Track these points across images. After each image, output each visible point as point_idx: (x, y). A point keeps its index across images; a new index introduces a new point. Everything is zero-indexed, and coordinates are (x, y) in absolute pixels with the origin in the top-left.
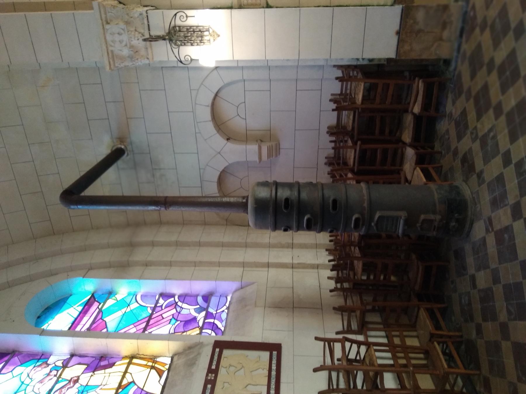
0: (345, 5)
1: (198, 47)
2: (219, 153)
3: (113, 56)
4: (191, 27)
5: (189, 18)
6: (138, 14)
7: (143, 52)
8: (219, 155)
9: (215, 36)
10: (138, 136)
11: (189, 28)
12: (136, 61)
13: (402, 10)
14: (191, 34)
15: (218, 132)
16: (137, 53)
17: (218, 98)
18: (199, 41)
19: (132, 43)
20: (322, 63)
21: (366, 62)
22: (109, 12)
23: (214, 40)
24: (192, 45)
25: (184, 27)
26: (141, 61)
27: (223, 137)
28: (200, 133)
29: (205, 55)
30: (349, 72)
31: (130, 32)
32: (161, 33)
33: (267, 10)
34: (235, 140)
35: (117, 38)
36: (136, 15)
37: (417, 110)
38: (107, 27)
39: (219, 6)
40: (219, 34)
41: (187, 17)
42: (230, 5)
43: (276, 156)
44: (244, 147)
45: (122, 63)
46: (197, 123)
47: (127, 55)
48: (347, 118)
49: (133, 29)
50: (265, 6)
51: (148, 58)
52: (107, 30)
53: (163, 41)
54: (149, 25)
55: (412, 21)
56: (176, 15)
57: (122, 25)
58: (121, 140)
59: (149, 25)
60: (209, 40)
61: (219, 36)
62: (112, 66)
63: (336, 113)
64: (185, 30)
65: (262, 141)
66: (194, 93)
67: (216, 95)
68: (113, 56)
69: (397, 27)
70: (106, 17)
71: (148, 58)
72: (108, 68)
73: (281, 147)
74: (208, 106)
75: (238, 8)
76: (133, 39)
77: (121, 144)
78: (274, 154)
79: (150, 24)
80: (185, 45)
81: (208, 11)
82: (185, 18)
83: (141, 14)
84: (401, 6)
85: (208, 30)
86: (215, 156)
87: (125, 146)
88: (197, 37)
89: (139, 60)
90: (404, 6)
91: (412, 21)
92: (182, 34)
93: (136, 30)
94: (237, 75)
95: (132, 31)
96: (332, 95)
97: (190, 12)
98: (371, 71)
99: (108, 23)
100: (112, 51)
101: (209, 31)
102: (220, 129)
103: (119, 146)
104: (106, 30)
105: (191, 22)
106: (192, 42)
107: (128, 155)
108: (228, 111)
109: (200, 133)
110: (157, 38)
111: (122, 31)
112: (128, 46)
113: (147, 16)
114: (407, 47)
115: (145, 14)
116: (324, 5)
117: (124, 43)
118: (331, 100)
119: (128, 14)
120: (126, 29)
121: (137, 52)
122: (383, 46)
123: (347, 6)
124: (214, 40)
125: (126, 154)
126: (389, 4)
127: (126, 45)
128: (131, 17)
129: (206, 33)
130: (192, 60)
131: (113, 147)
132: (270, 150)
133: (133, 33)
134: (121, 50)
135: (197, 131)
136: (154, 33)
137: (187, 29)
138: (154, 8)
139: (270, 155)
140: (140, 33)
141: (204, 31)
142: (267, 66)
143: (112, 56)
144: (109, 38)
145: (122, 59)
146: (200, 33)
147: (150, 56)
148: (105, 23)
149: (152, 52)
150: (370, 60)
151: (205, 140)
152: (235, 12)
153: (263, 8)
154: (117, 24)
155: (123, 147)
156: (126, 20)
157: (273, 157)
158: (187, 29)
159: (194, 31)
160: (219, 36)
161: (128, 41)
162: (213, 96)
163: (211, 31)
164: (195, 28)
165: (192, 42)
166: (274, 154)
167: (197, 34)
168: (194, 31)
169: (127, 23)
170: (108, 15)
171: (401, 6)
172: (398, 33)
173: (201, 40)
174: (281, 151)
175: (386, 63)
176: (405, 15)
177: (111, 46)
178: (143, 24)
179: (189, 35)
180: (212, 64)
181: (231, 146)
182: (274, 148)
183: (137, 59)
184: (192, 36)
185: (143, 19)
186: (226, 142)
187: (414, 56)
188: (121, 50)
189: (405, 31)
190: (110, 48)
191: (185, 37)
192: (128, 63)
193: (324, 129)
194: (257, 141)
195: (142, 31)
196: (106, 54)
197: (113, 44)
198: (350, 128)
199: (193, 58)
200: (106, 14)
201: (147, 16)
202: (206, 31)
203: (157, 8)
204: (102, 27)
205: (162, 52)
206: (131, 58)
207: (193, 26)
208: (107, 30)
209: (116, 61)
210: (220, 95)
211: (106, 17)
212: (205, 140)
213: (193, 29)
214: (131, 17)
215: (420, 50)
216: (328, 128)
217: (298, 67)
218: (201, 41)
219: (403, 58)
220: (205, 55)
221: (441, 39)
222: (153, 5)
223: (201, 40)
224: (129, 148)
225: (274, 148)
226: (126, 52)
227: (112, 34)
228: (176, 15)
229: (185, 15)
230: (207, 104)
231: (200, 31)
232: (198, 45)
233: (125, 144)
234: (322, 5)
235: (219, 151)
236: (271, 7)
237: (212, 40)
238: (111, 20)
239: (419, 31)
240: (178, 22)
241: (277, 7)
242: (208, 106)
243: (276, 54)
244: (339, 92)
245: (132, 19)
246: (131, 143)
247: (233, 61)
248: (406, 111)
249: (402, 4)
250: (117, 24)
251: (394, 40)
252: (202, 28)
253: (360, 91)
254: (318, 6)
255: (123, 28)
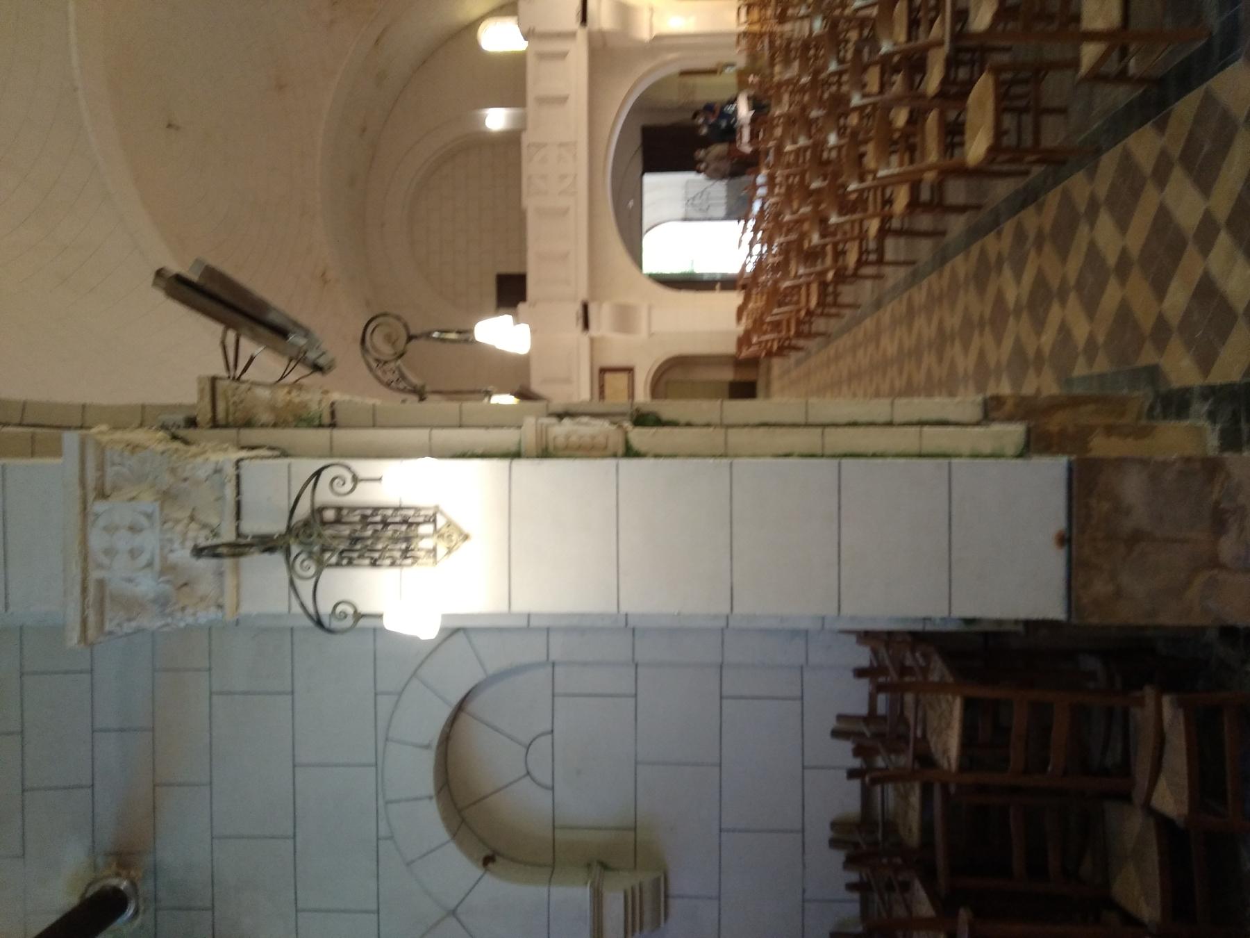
0: (871, 451)
1: (395, 571)
2: (453, 913)
3: (101, 602)
4: (376, 510)
5: (360, 486)
6: (210, 468)
7: (206, 586)
8: (452, 921)
9: (455, 537)
10: (181, 848)
11: (369, 512)
12: (179, 615)
13: (1070, 470)
14: (376, 531)
15: (454, 835)
16: (186, 589)
17: (463, 717)
18: (397, 554)
19: (173, 558)
20: (803, 625)
21: (951, 627)
22: (113, 464)
23: (450, 550)
24: (374, 564)
25: (353, 509)
26: (194, 614)
27: (470, 855)
28: (391, 838)
29: (405, 601)
30: (902, 658)
31: (167, 526)
32: (276, 526)
33: (626, 464)
34: (513, 860)
35: (123, 541)
36: (202, 473)
37: (1170, 798)
38: (99, 507)
39: (480, 451)
40: (466, 530)
41: (356, 480)
42: (514, 449)
43: (656, 924)
44: (543, 890)
45: (129, 620)
46: (387, 803)
47: (152, 595)
48: (906, 807)
49: (184, 514)
50: (621, 450)
51: (220, 607)
52: (97, 516)
53: (266, 556)
54: (238, 505)
55: (1106, 506)
56: (318, 474)
57: (148, 502)
58: (123, 859)
59: (238, 505)
60: (434, 550)
61: (466, 537)
62: (91, 632)
63: (856, 784)
64: (357, 518)
65: (605, 866)
66: (385, 703)
67: (460, 708)
68: (101, 602)
69: (1058, 522)
70: (101, 478)
71: (220, 607)
72: (74, 637)
73: (674, 889)
74: (427, 747)
75: (538, 457)
76: (176, 545)
77: (118, 875)
78: (647, 917)
79: (246, 498)
80: (350, 563)
81: (428, 461)
82: (349, 486)
83: (218, 471)
84: (1063, 461)
85: (432, 520)
86: (438, 922)
87: (133, 884)
88: (395, 540)
89: (190, 610)
90: (1073, 458)
91: (1106, 506)
92: (346, 530)
93: (192, 518)
94: (533, 651)
95: (177, 521)
96: (840, 717)
97: (364, 467)
98: (977, 655)
99: (102, 495)
100: (101, 584)
101: (435, 521)
102: (463, 820)
103: (114, 882)
104: (91, 518)
105: (369, 495)
106: (376, 555)
107: (136, 912)
108: (494, 758)
109: (391, 838)
110: (267, 544)
111: (144, 521)
112: (157, 565)
113: (238, 477)
114: (1101, 587)
115: (230, 471)
116: (806, 452)
117: (143, 559)
118: (836, 734)
119: (173, 471)
120: (157, 514)
121: (186, 584)
122: (1021, 583)
123: (874, 455)
124: (450, 550)
125: (130, 911)
126: (1011, 449)
127: (150, 564)
128: (185, 480)
129: (425, 529)
130: (358, 616)
131: (90, 885)
132: (633, 906)
133: (179, 528)
134: (130, 580)
135: (384, 831)
136: (253, 526)
137: (364, 517)
138: (276, 453)
139: (632, 921)
140: (204, 526)
141: (418, 524)
142: (629, 629)
143: (97, 598)
144: (97, 541)
145: (132, 606)
146: (404, 528)
147: (229, 600)
148: (91, 496)
149: (238, 587)
150: (969, 621)
151: (408, 864)
152: (523, 467)
153: (615, 456)
154: (133, 499)
155: (124, 885)
156: (165, 488)
157: (646, 931)
158: (364, 517)
159: (385, 523)
160: (466, 537)
161: (157, 551)
162: (445, 713)
163: (441, 521)
164: (389, 512)
165: (376, 555)
166: (647, 917)
167: (395, 531)
168: (385, 523)
169: (167, 496)
170: (110, 471)
171: (1063, 461)
172: (1064, 540)
173: (407, 550)
174: (676, 906)
175: (1020, 628)
176: (1084, 484)
177: (100, 566)
178: (220, 498)
179: (369, 533)
180: (428, 631)
181: (497, 888)
182: (648, 897)
183: (183, 609)
184: (376, 536)
185: (223, 485)
186: (476, 871)
187: (1128, 614)
188: (130, 580)
189: (1089, 530)
190: (95, 575)
191: (355, 540)
192: (151, 622)
193: (821, 832)
194: (589, 865)
195: (214, 521)
196: (77, 590)
197: (105, 561)
198: (912, 832)
199: (363, 609)
200: (101, 467)
201: (238, 477)
202: (425, 522)
203: (285, 454)
204: (77, 508)
205: (265, 586)
206: (162, 603)
207: (387, 508)
208: (97, 516)
209: (109, 614)
210: (472, 707)
211: (101, 478)
212: (408, 864)
213: (384, 517)
214: (185, 480)
215: (1143, 597)
216: (834, 825)
217: (725, 630)
218: (405, 553)
219: (1094, 620)
220: (405, 601)
221: (1214, 562)
222: (273, 444)
223: (407, 550)
224: (145, 888)
225: (648, 897)
226: (147, 586)
227: (110, 529)
228: (318, 474)
229: (349, 477)
230: (426, 742)
231: (405, 521)
232: (393, 564)
233: (133, 873)
234: (797, 450)
235: (452, 904)
236: (637, 455)
237: (442, 549)
238: (115, 488)
239: (1136, 537)
240: (324, 495)
241: (657, 456)
242: (427, 747)
243: (646, 599)
244: (863, 710)
245: (186, 485)
246: (155, 871)
247: (510, 614)
248: (1125, 797)
249: (1070, 453)
250: (133, 499)
251: (1056, 561)
252: (411, 512)
253: (949, 725)
254: (787, 455)
255: (149, 510)
